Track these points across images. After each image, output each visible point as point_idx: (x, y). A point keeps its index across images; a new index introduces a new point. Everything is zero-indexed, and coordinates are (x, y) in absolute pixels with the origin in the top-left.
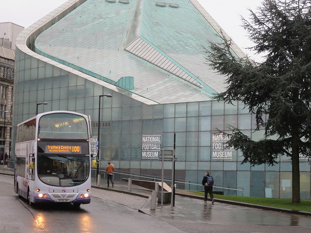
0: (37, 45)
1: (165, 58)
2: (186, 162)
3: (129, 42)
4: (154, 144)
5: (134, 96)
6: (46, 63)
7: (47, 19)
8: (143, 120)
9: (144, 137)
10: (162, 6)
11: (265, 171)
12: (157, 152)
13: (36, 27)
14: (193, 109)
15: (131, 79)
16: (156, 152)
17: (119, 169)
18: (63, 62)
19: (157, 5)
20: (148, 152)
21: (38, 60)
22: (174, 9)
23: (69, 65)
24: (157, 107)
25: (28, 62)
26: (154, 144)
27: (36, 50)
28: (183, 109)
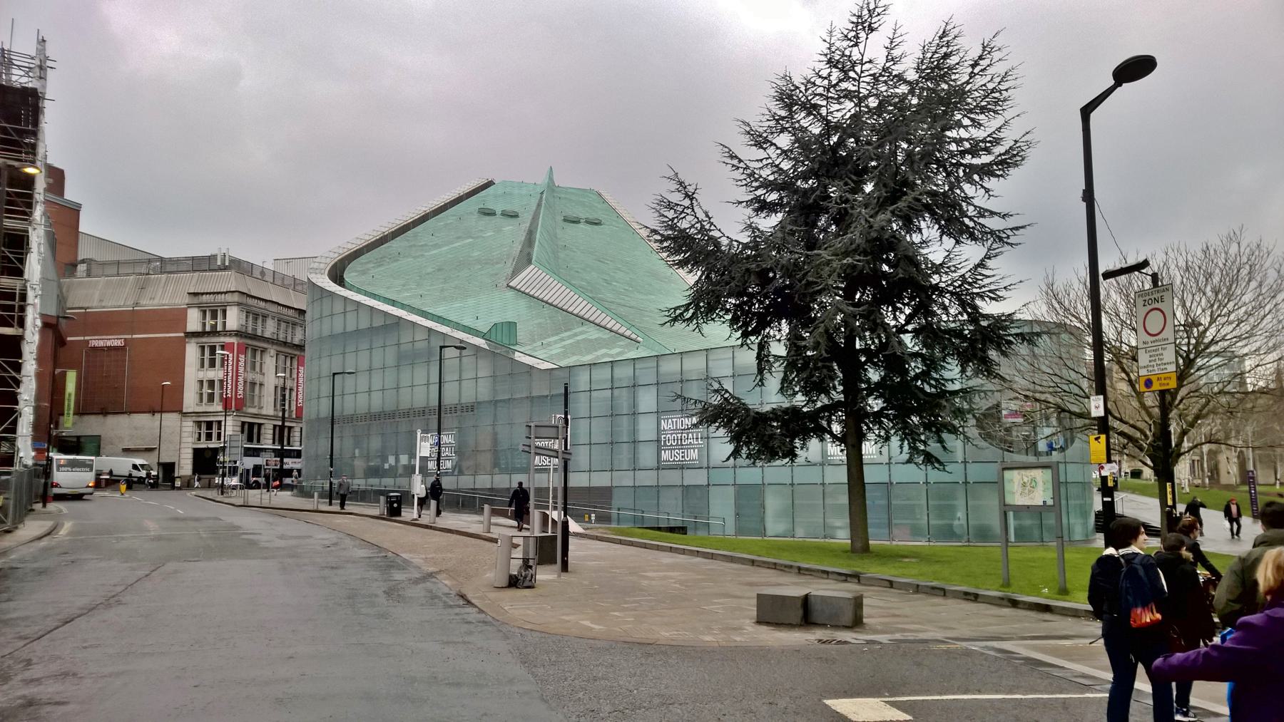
0: (348, 277)
1: (576, 296)
2: (636, 472)
3: (515, 273)
4: (688, 434)
5: (518, 357)
6: (358, 303)
7: (371, 237)
8: (496, 401)
9: (664, 419)
10: (574, 222)
11: (764, 484)
12: (696, 450)
13: (350, 247)
14: (624, 373)
15: (512, 326)
16: (694, 449)
17: (491, 489)
18: (393, 303)
19: (565, 220)
20: (674, 449)
21: (346, 298)
22: (596, 227)
23: (403, 306)
24: (556, 372)
25: (327, 302)
26: (688, 434)
27: (346, 284)
28: (603, 374)
